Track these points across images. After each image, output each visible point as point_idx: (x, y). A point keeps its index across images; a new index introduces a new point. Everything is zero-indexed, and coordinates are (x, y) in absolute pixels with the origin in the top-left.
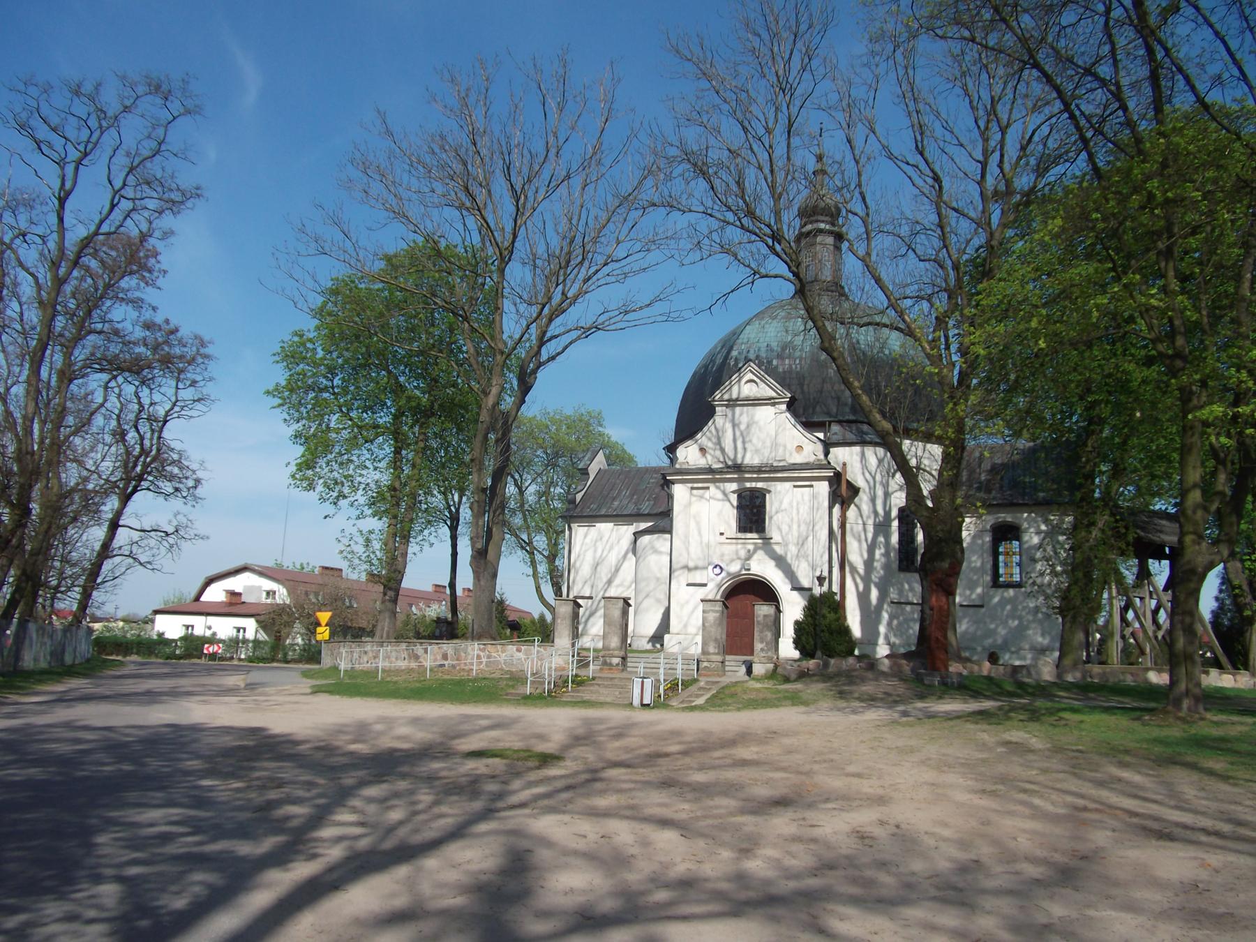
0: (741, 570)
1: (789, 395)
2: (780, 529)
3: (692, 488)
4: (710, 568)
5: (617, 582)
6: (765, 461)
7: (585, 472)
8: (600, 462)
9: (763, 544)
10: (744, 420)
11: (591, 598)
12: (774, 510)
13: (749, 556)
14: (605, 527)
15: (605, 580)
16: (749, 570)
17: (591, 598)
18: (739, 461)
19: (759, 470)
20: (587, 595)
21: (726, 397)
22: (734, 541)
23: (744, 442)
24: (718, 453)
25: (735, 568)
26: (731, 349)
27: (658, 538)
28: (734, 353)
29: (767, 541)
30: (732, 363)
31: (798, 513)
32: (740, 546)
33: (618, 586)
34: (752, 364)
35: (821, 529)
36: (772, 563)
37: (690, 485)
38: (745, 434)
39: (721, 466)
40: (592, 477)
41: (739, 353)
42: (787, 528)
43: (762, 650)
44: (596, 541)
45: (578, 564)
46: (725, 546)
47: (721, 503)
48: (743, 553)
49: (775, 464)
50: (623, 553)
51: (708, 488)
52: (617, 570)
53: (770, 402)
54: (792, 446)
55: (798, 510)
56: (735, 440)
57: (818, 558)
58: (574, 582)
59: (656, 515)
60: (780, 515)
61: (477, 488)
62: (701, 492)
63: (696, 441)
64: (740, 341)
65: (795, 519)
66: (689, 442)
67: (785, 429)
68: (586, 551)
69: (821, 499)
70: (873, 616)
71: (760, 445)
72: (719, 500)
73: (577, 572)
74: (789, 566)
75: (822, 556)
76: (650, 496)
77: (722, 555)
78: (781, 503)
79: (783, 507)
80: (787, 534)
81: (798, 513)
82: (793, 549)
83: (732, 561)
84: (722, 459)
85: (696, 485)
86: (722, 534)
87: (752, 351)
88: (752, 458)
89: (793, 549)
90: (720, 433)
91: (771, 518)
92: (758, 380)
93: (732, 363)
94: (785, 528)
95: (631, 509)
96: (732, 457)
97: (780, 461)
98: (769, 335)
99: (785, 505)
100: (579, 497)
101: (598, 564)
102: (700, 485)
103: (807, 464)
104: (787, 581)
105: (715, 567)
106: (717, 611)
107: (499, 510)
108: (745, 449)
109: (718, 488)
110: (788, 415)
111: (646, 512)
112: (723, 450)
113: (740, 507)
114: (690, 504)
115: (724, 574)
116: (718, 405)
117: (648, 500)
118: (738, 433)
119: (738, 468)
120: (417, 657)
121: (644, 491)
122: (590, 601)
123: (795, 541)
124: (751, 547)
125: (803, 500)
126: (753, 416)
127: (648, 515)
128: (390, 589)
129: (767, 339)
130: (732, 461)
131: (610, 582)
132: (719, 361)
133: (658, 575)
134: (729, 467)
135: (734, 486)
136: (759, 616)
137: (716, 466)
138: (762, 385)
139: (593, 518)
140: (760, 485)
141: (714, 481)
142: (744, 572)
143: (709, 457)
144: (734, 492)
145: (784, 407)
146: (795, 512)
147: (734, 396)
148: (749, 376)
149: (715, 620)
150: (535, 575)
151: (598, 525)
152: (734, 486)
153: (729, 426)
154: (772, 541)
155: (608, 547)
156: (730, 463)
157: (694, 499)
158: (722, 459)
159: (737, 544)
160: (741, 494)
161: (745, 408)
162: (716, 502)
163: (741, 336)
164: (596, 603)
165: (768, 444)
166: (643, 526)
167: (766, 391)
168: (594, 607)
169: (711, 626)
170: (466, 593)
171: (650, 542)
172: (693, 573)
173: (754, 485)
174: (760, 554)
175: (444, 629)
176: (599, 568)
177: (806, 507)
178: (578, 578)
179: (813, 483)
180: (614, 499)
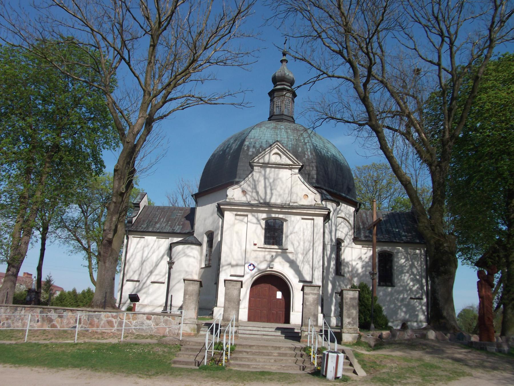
0: (267, 268)
1: (301, 164)
2: (293, 244)
3: (236, 215)
4: (247, 265)
5: (156, 272)
6: (284, 202)
7: (137, 206)
8: (145, 201)
9: (282, 252)
10: (272, 175)
11: (138, 281)
12: (289, 232)
13: (273, 260)
14: (151, 239)
15: (148, 270)
16: (272, 268)
17: (138, 281)
18: (268, 201)
19: (282, 207)
20: (136, 279)
21: (261, 161)
22: (264, 250)
23: (271, 190)
24: (254, 194)
25: (263, 266)
26: (244, 140)
27: (188, 247)
28: (246, 143)
29: (284, 251)
30: (246, 149)
31: (304, 235)
32: (266, 253)
33: (157, 275)
34: (278, 144)
35: (319, 245)
36: (287, 265)
37: (235, 213)
38: (272, 184)
39: (256, 202)
40: (141, 209)
41: (250, 143)
42: (297, 244)
43: (349, 323)
44: (144, 248)
45: (131, 260)
46: (258, 252)
47: (255, 225)
48: (268, 257)
49: (291, 204)
50: (161, 255)
51: (247, 216)
52: (157, 265)
53: (289, 167)
54: (301, 194)
55: (304, 233)
56: (265, 187)
57: (317, 263)
58: (127, 271)
59: (185, 234)
60: (293, 235)
61: (117, 192)
62: (241, 218)
63: (240, 186)
64: (249, 137)
65: (302, 238)
66: (236, 186)
67: (297, 184)
68: (137, 253)
69: (319, 228)
70: (329, 300)
71: (282, 192)
72: (254, 223)
73: (130, 265)
74: (298, 267)
75: (319, 262)
76: (180, 222)
77: (256, 258)
78: (294, 228)
79: (295, 231)
80: (298, 247)
81: (304, 235)
82: (300, 257)
83: (261, 262)
84: (257, 199)
85: (239, 213)
86: (255, 245)
87: (257, 143)
88: (277, 200)
89: (300, 257)
90: (257, 183)
91: (287, 237)
92: (281, 154)
93: (246, 149)
94: (296, 244)
95: (168, 229)
96: (263, 198)
97: (294, 202)
98: (266, 135)
99: (296, 230)
100: (134, 219)
101: (144, 261)
102: (242, 213)
103: (311, 206)
104: (296, 276)
105: (250, 265)
106: (315, 294)
107: (124, 212)
108: (272, 194)
109: (254, 216)
110: (299, 175)
111: (179, 231)
112: (257, 193)
113: (266, 230)
114: (234, 224)
115: (255, 270)
116: (256, 166)
117: (179, 225)
118: (268, 184)
119: (267, 204)
120: (50, 320)
121: (175, 220)
122: (138, 283)
123: (302, 252)
124: (274, 254)
125: (307, 227)
126: (278, 175)
127: (180, 233)
128: (13, 267)
129: (266, 138)
130: (263, 200)
131: (151, 272)
132: (235, 147)
133: (187, 269)
134: (261, 203)
135: (264, 216)
136: (347, 298)
137: (253, 202)
138: (284, 157)
139: (143, 233)
140: (281, 216)
141: (251, 211)
142: (269, 269)
143: (248, 197)
144: (263, 219)
145: (297, 171)
146: (302, 234)
147: (266, 161)
148: (276, 150)
149: (314, 301)
150: (90, 267)
151: (146, 237)
152: (264, 216)
153: (262, 179)
154: (287, 251)
155: (152, 251)
156: (262, 201)
157: (237, 221)
158: (257, 198)
159: (265, 251)
160: (268, 221)
161: (273, 169)
162: (252, 225)
163: (250, 135)
164: (141, 285)
165: (287, 192)
166: (176, 240)
167: (285, 160)
168: (140, 287)
169: (311, 305)
170: (26, 275)
171: (183, 249)
172: (235, 268)
173: (277, 216)
174: (279, 259)
175: (33, 296)
176: (145, 264)
177: (309, 232)
178: (130, 269)
179: (314, 217)
180: (156, 223)
